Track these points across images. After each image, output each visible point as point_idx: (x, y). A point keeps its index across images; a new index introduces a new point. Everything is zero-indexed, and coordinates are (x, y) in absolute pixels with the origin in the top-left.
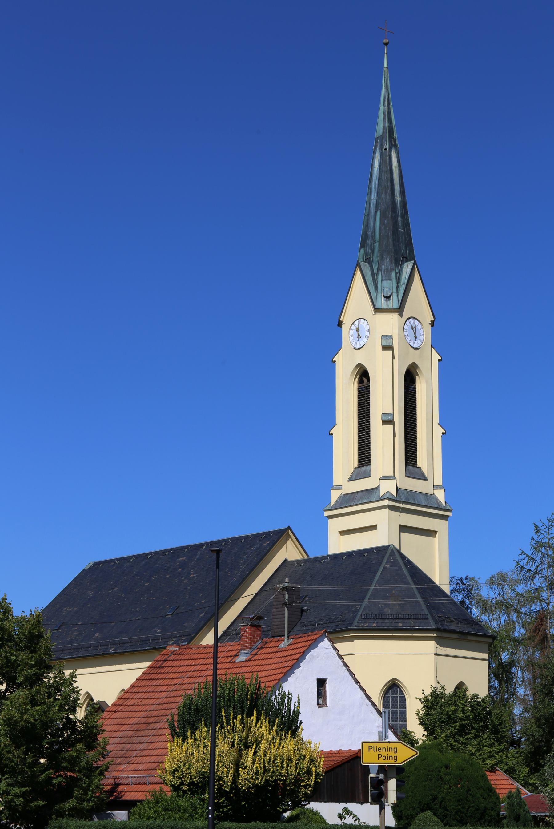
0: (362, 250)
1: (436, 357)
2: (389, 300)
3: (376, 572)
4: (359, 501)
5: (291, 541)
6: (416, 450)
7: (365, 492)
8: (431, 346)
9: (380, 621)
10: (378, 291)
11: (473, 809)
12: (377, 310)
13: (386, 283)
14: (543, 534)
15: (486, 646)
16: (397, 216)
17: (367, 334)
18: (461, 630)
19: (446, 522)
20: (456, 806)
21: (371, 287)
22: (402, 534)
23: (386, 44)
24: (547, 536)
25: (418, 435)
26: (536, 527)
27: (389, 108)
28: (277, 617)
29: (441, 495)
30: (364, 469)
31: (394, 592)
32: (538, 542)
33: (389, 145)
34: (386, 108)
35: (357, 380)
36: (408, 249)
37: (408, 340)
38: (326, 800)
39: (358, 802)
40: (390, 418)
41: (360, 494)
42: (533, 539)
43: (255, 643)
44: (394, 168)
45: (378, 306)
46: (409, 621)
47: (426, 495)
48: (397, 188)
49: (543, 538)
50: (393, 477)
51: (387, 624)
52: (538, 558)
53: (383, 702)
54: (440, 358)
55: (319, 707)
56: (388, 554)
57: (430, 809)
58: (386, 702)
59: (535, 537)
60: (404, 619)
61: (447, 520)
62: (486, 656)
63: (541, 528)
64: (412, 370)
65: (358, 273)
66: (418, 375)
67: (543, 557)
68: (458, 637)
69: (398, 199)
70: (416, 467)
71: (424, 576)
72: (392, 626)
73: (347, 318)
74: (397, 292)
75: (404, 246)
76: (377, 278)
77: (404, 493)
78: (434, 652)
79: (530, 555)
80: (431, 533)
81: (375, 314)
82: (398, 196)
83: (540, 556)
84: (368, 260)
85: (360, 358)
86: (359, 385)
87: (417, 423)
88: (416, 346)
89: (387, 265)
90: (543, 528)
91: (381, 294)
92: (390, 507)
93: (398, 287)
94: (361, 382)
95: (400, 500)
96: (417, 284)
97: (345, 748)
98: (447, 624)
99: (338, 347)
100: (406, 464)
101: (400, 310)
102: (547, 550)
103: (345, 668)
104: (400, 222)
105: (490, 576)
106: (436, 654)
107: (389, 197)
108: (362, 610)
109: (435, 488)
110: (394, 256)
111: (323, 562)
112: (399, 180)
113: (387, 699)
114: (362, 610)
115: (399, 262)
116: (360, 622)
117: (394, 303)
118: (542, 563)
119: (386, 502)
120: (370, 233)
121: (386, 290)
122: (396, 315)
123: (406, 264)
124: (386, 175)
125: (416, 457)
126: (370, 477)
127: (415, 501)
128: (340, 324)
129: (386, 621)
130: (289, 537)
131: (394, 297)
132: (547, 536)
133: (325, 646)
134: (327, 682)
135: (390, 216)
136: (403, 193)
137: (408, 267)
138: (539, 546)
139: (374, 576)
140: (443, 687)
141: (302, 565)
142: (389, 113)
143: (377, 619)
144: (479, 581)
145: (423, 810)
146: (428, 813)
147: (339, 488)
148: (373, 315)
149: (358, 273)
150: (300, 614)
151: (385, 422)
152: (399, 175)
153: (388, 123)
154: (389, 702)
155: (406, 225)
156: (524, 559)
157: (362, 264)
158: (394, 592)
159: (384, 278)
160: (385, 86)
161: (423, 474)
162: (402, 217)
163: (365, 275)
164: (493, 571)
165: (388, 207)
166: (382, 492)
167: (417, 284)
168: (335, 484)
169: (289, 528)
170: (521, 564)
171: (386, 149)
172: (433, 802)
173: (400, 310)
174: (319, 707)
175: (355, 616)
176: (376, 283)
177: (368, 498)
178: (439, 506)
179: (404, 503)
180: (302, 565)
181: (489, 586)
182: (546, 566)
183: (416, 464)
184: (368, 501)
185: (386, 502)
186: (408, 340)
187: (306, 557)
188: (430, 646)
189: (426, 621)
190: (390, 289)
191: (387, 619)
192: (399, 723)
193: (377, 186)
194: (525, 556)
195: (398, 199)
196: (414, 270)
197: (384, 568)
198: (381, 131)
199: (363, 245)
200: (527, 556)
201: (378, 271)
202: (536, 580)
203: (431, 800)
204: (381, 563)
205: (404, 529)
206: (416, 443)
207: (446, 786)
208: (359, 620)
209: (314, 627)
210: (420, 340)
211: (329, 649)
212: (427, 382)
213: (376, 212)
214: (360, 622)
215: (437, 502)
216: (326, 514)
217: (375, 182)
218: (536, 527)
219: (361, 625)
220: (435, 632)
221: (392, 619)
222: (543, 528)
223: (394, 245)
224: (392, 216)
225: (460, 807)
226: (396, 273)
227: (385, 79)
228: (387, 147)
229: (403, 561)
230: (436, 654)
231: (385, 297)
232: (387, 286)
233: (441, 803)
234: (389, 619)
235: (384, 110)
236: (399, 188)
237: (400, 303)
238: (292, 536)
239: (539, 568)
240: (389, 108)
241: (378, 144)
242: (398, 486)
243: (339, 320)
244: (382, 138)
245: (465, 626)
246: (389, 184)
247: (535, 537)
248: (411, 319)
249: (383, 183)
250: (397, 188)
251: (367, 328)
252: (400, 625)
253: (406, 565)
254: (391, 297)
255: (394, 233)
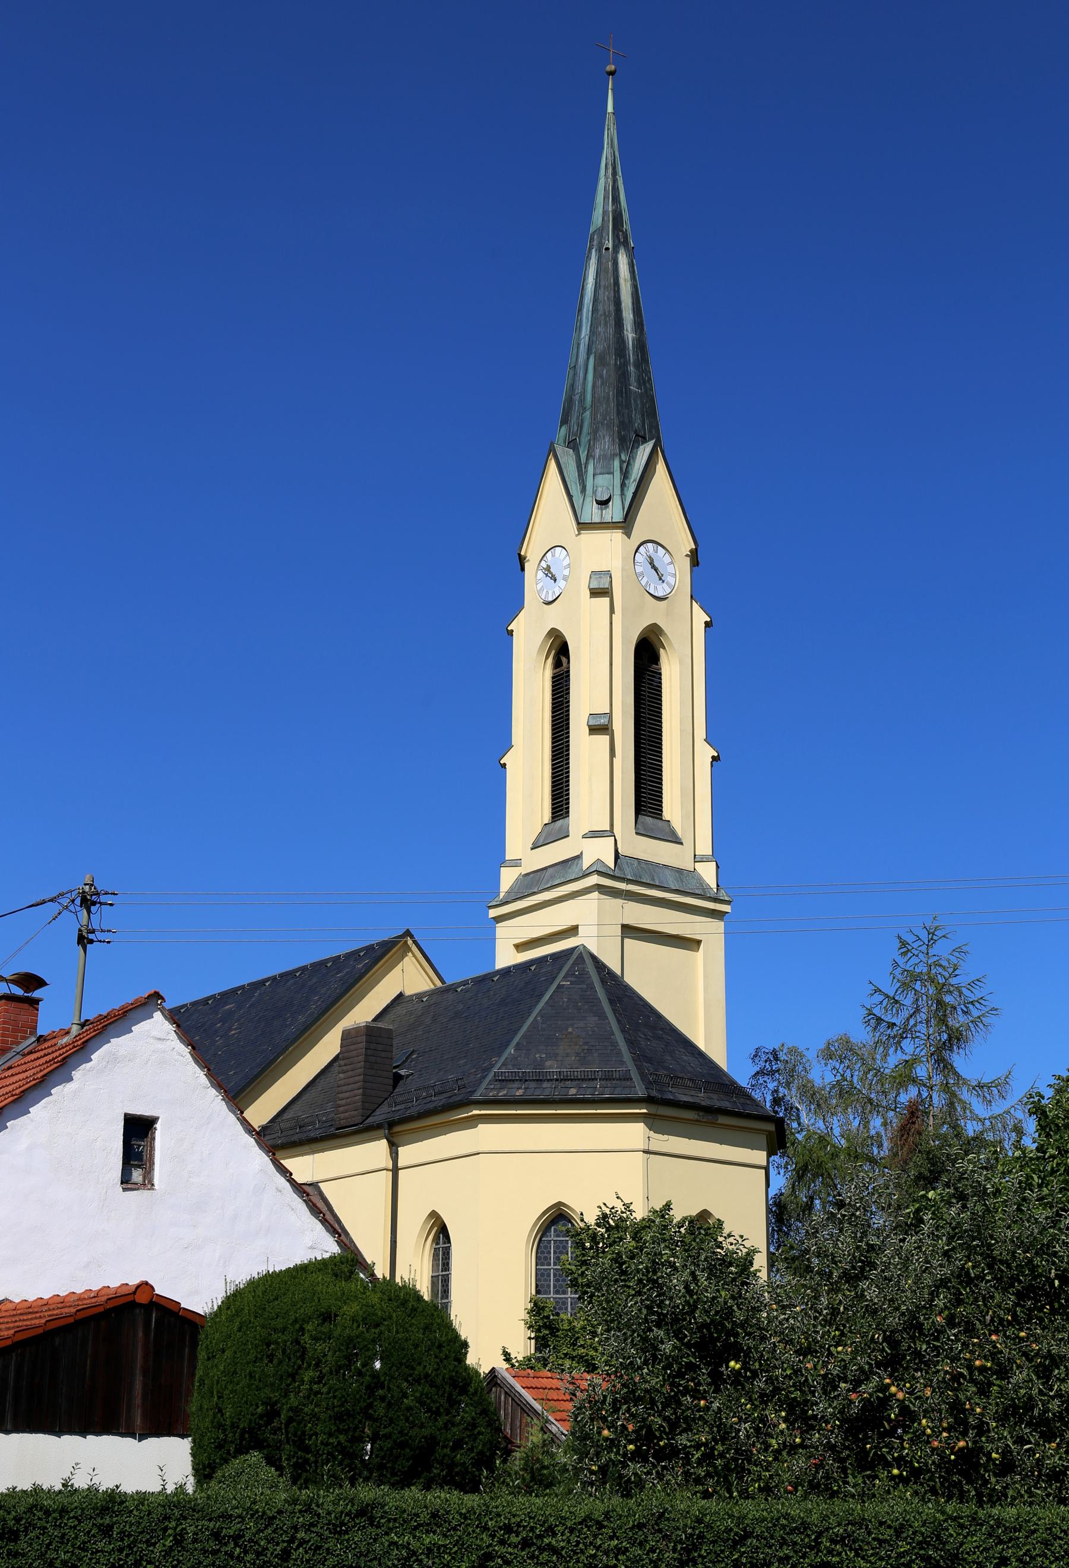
0: (564, 429)
1: (701, 617)
2: (606, 508)
3: (541, 995)
4: (548, 882)
5: (413, 958)
6: (661, 788)
7: (559, 866)
8: (692, 597)
9: (533, 1085)
10: (587, 493)
11: (388, 1444)
12: (583, 526)
13: (602, 480)
14: (917, 956)
15: (763, 1140)
16: (626, 363)
17: (566, 572)
18: (703, 1103)
19: (719, 926)
20: (330, 1435)
21: (574, 488)
22: (626, 941)
23: (612, 73)
24: (925, 960)
25: (664, 760)
26: (904, 944)
27: (615, 181)
28: (345, 1088)
29: (708, 873)
30: (559, 823)
31: (570, 1030)
32: (907, 971)
33: (614, 242)
34: (610, 181)
35: (550, 660)
36: (647, 422)
37: (644, 582)
38: (9, 1427)
39: (129, 1433)
40: (603, 721)
41: (550, 870)
42: (896, 965)
43: (18, 1043)
44: (622, 281)
45: (585, 518)
46: (591, 1084)
47: (680, 871)
48: (628, 315)
49: (916, 964)
50: (611, 833)
51: (547, 1090)
52: (908, 1000)
53: (537, 1253)
54: (709, 619)
55: (124, 1190)
56: (571, 962)
57: (259, 1445)
58: (543, 1252)
59: (901, 961)
60: (583, 1080)
61: (722, 920)
62: (760, 1157)
63: (913, 945)
64: (653, 639)
65: (552, 466)
66: (664, 648)
67: (917, 1000)
68: (696, 1117)
69: (630, 335)
70: (661, 819)
71: (641, 1003)
72: (557, 1095)
73: (532, 549)
74: (622, 494)
75: (638, 416)
76: (586, 471)
77: (632, 865)
78: (642, 1147)
79: (891, 996)
80: (691, 944)
81: (579, 534)
82: (629, 329)
83: (911, 996)
84: (572, 444)
85: (554, 618)
86: (555, 671)
87: (664, 738)
88: (660, 593)
89: (604, 447)
90: (915, 945)
91: (591, 498)
92: (599, 888)
93: (623, 485)
94: (557, 664)
95: (622, 876)
96: (661, 481)
97: (114, 1284)
98: (674, 1090)
99: (518, 605)
100: (638, 811)
101: (626, 524)
102: (925, 986)
103: (214, 1091)
104: (633, 374)
105: (825, 1041)
106: (645, 1152)
107: (611, 331)
108: (499, 1065)
109: (697, 859)
110: (619, 432)
111: (459, 990)
112: (633, 304)
113: (546, 1247)
114: (499, 1065)
115: (628, 442)
116: (492, 1087)
117: (615, 512)
118: (917, 1010)
119: (594, 879)
120: (577, 397)
121: (600, 489)
122: (618, 535)
123: (641, 447)
124: (607, 293)
125: (661, 802)
126: (568, 836)
127: (653, 880)
128: (522, 560)
129: (545, 1085)
130: (409, 949)
131: (616, 502)
132: (925, 960)
133: (155, 1033)
134: (158, 1126)
135: (612, 362)
136: (639, 325)
137: (644, 452)
138: (908, 982)
139: (538, 1002)
140: (627, 1206)
141: (425, 1000)
142: (615, 189)
143: (526, 1081)
144: (805, 1053)
145: (241, 1450)
146: (255, 1457)
147: (516, 863)
148: (577, 535)
149: (552, 466)
150: (391, 1082)
151: (594, 730)
152: (632, 294)
153: (613, 204)
154: (550, 1253)
155: (644, 381)
156: (881, 1003)
157: (560, 449)
158: (570, 1030)
159: (598, 471)
160: (608, 144)
161: (673, 833)
162: (637, 365)
163: (563, 467)
164: (831, 1032)
165: (609, 347)
166: (586, 863)
167: (661, 481)
168: (509, 856)
169: (408, 933)
170: (876, 1011)
171: (607, 249)
172: (270, 1422)
173: (626, 524)
174: (124, 1190)
175: (484, 1077)
176: (583, 480)
177: (563, 877)
178: (705, 892)
179: (629, 881)
180: (425, 1000)
181: (823, 1062)
182: (924, 1016)
183: (661, 815)
184: (563, 880)
185: (594, 879)
186: (644, 582)
187: (439, 984)
188: (635, 1133)
189: (628, 1083)
190: (608, 488)
191: (548, 1080)
192: (569, 1295)
193: (590, 313)
194: (882, 997)
195: (630, 335)
196: (655, 456)
197: (559, 987)
198: (600, 219)
199: (565, 421)
200: (888, 996)
201: (587, 459)
202: (905, 1043)
203: (261, 1417)
204: (554, 979)
205: (629, 931)
206: (661, 775)
207: (308, 1375)
208: (490, 1083)
209: (410, 1105)
210: (668, 584)
211: (168, 1043)
212: (681, 662)
213: (588, 358)
214: (492, 1087)
215: (701, 884)
216: (493, 913)
217: (588, 307)
218: (904, 944)
219: (491, 1094)
220: (644, 1105)
221: (557, 1080)
222: (915, 945)
223: (618, 413)
224: (616, 363)
225: (342, 1438)
226: (622, 462)
227: (610, 132)
228: (610, 246)
229: (599, 973)
230: (645, 1152)
231: (599, 503)
232: (605, 483)
233: (287, 1425)
234: (551, 1080)
235: (605, 184)
236: (632, 316)
237: (626, 510)
238: (414, 948)
239: (912, 1022)
240: (615, 181)
241: (595, 243)
242: (620, 851)
243: (519, 555)
244: (601, 230)
245: (715, 1096)
246: (612, 308)
247: (901, 961)
248: (650, 545)
249: (600, 308)
250: (628, 315)
251: (566, 562)
252: (573, 1091)
253: (603, 981)
254: (611, 503)
255: (619, 393)
